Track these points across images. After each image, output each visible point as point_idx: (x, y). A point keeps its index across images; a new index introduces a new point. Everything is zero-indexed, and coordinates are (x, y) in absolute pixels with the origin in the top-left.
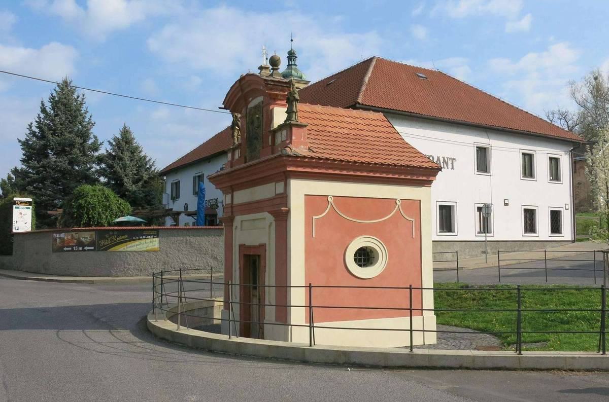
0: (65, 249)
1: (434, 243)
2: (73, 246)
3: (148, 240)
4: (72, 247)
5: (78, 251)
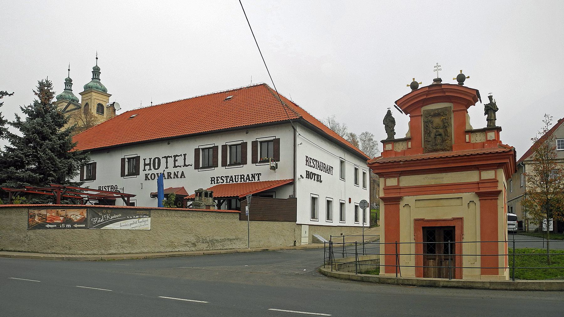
0: (48, 226)
1: (417, 221)
2: (59, 224)
3: (141, 220)
4: (58, 224)
5: (65, 228)
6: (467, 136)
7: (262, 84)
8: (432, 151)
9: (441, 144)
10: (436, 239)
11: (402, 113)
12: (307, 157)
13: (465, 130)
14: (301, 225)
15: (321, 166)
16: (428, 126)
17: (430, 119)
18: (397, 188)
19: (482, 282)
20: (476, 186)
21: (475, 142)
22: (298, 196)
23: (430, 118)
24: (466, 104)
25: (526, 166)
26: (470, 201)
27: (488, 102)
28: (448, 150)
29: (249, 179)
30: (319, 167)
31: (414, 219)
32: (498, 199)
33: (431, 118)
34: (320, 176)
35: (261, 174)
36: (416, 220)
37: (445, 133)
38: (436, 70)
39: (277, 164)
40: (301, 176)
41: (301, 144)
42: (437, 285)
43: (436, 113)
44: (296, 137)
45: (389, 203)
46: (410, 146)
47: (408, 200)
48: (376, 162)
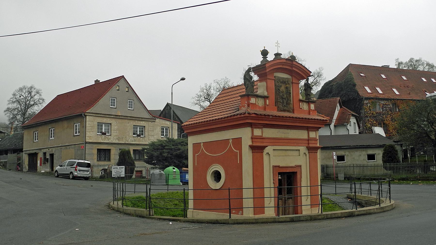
18: (261, 138)
25: (87, 117)
36: (274, 167)
47: (269, 149)
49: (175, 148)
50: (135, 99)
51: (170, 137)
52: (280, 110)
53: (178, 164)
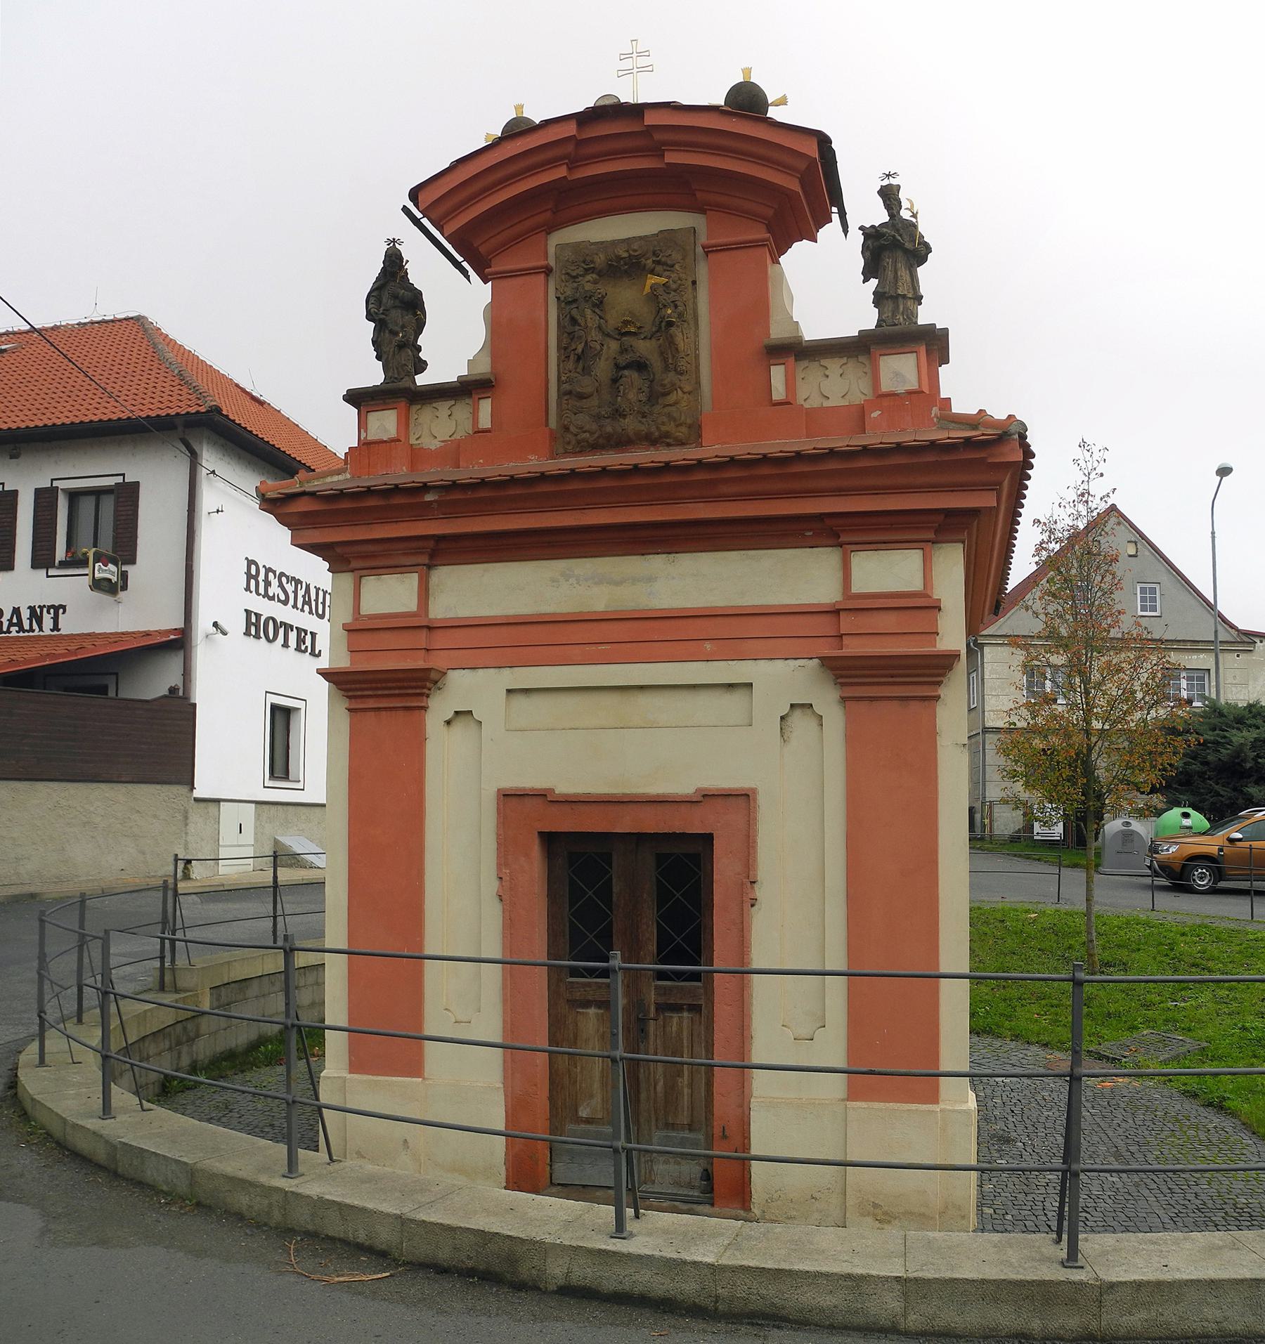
6: (778, 374)
7: (132, 318)
8: (595, 447)
9: (646, 409)
10: (614, 899)
11: (468, 277)
12: (250, 562)
13: (766, 342)
14: (217, 801)
15: (317, 600)
16: (578, 317)
17: (588, 287)
19: (849, 1277)
20: (823, 625)
21: (815, 402)
22: (201, 696)
23: (587, 283)
24: (770, 212)
25: (986, 649)
26: (792, 706)
27: (879, 216)
28: (676, 439)
29: (20, 624)
30: (307, 602)
31: (499, 790)
32: (939, 697)
33: (595, 282)
34: (313, 635)
35: (64, 607)
36: (509, 798)
37: (665, 360)
38: (629, 72)
39: (124, 576)
40: (215, 625)
41: (218, 511)
42: (525, 1271)
43: (619, 258)
44: (198, 477)
45: (371, 703)
46: (485, 421)
48: (304, 494)
49: (1219, 740)
50: (1165, 578)
51: (1214, 696)
52: (579, 442)
53: (1230, 798)
